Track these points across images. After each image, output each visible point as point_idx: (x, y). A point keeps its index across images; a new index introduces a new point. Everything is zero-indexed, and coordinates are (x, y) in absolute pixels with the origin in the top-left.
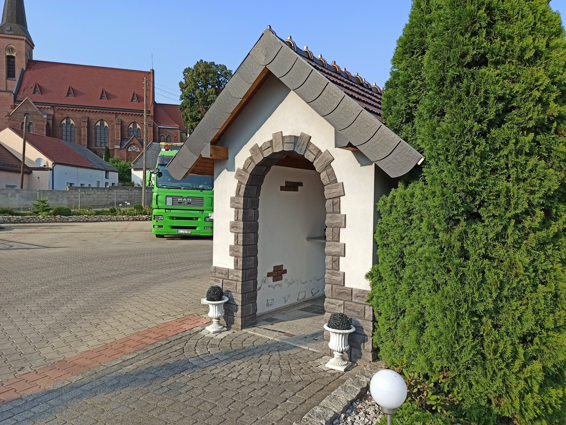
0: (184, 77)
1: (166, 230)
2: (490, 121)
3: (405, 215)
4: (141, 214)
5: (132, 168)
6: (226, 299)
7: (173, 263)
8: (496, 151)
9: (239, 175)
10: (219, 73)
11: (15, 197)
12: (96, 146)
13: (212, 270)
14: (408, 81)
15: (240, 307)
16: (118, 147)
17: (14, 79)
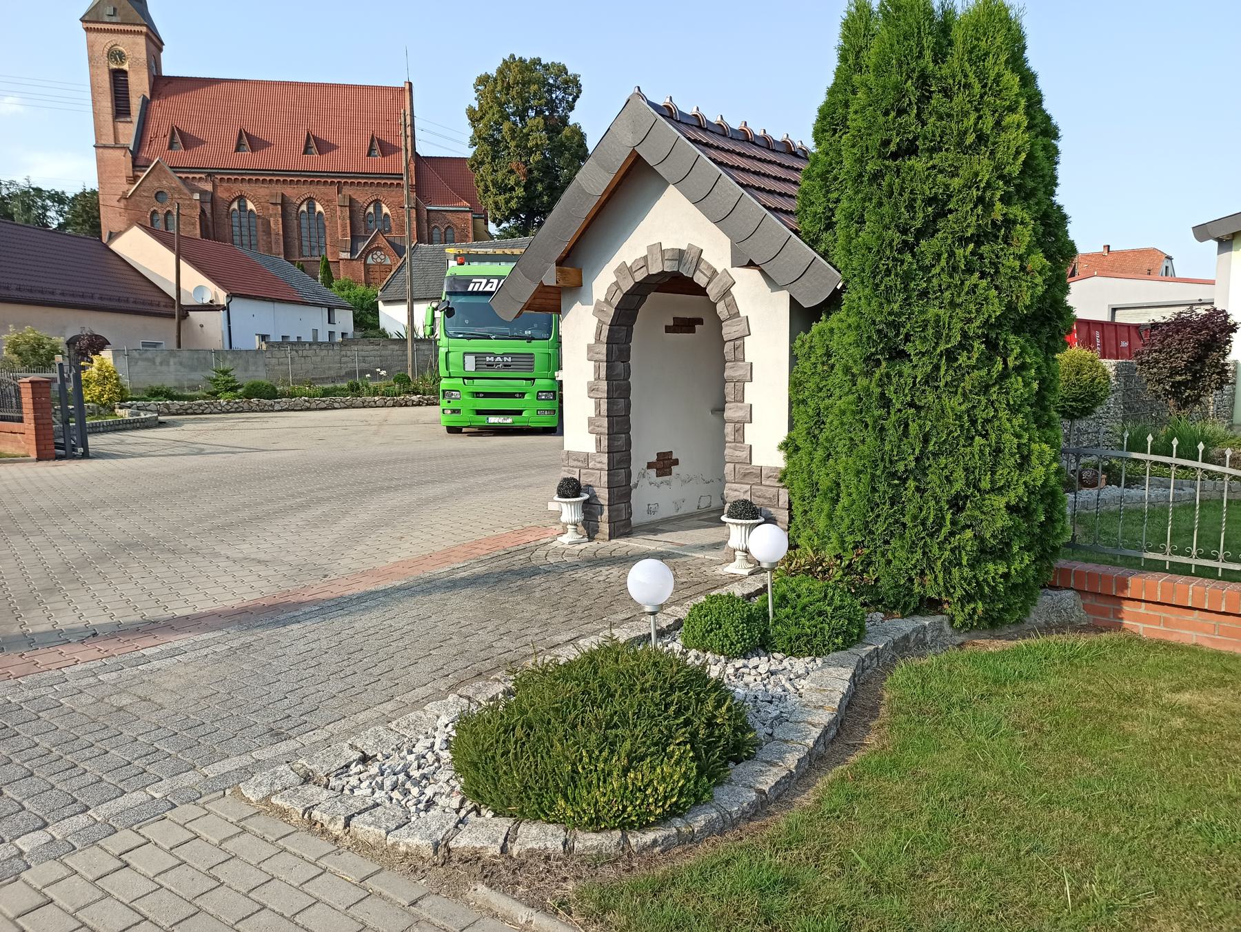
0: (476, 95)
1: (466, 418)
2: (918, 230)
3: (825, 359)
4: (408, 392)
5: (380, 299)
6: (586, 496)
7: (489, 469)
8: (926, 269)
9: (598, 311)
10: (551, 81)
11: (168, 364)
12: (301, 255)
13: (564, 457)
14: (828, 172)
15: (606, 508)
16: (346, 255)
17: (129, 119)
